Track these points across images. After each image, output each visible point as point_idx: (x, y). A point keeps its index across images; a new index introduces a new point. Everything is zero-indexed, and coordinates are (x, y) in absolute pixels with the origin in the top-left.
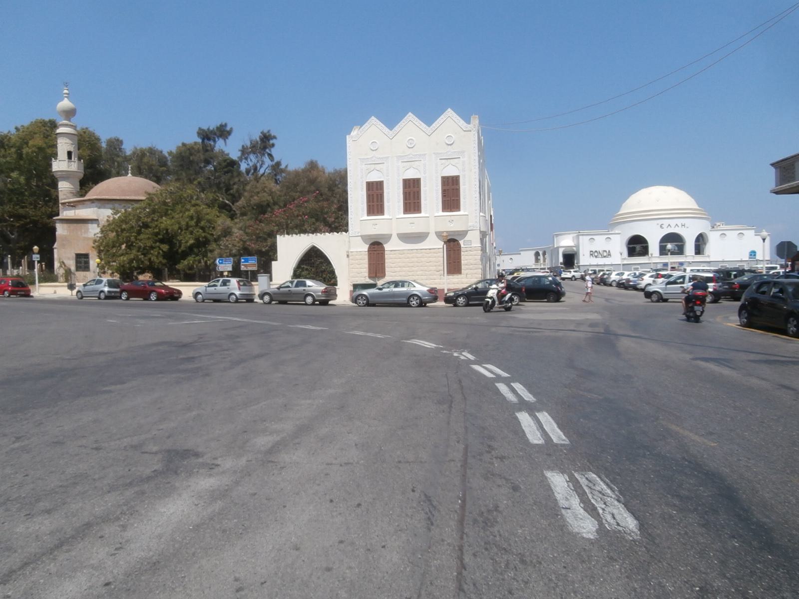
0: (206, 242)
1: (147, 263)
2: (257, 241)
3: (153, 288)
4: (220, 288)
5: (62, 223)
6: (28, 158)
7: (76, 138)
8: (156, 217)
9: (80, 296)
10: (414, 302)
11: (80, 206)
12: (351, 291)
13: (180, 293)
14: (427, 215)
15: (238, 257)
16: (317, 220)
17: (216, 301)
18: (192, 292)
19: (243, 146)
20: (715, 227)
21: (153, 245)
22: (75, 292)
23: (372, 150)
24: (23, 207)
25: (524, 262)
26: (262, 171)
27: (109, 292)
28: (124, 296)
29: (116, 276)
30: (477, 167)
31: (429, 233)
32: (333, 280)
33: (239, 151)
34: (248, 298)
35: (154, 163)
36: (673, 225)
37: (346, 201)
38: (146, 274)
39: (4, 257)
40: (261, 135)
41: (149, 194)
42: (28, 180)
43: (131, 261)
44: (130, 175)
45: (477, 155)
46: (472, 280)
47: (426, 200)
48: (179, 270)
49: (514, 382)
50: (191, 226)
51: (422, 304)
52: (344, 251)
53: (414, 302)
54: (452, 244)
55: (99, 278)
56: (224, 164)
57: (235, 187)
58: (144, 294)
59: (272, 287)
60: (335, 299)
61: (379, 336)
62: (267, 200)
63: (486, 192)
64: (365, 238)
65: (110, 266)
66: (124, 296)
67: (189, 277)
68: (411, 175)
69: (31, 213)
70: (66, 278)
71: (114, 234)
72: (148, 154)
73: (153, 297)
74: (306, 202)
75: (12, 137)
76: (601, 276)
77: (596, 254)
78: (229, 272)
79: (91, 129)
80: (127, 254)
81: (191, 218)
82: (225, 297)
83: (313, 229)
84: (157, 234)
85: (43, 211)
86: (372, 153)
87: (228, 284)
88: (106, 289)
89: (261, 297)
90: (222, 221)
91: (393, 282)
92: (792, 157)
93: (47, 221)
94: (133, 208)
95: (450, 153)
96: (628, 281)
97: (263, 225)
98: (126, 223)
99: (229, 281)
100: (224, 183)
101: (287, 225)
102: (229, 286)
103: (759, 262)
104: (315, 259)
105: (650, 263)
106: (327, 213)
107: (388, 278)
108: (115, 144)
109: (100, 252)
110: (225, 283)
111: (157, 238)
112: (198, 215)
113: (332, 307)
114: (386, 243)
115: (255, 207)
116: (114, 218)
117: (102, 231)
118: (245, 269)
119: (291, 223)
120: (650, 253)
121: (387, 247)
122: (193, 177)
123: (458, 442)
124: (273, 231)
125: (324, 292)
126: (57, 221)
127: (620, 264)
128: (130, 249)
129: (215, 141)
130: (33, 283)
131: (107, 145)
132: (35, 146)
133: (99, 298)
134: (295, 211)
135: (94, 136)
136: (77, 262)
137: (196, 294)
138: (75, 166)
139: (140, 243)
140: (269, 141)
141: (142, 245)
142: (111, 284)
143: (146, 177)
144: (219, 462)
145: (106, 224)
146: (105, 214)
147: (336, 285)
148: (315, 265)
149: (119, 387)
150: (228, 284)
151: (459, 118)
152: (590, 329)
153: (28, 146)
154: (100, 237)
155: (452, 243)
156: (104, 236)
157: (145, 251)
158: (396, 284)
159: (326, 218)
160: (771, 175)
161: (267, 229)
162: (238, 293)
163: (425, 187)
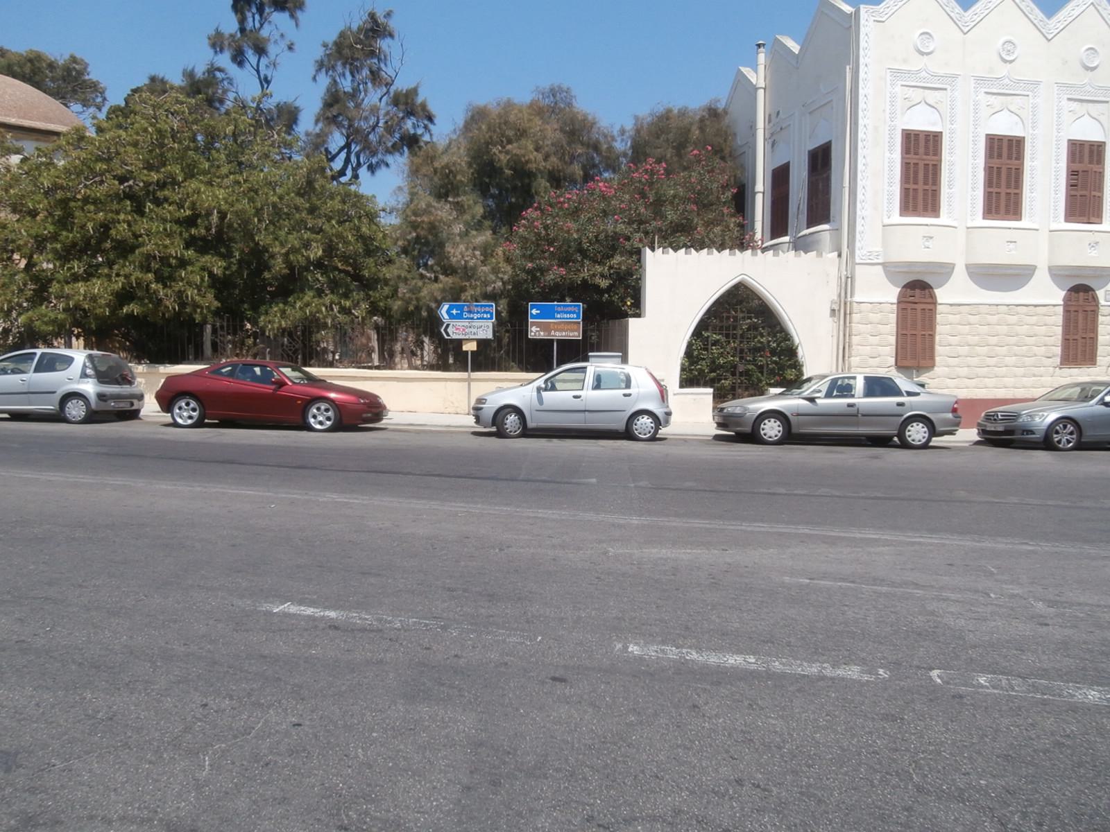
47: (950, 186)
64: (891, 270)
114: (940, 286)
121: (942, 295)
163: (1032, 159)
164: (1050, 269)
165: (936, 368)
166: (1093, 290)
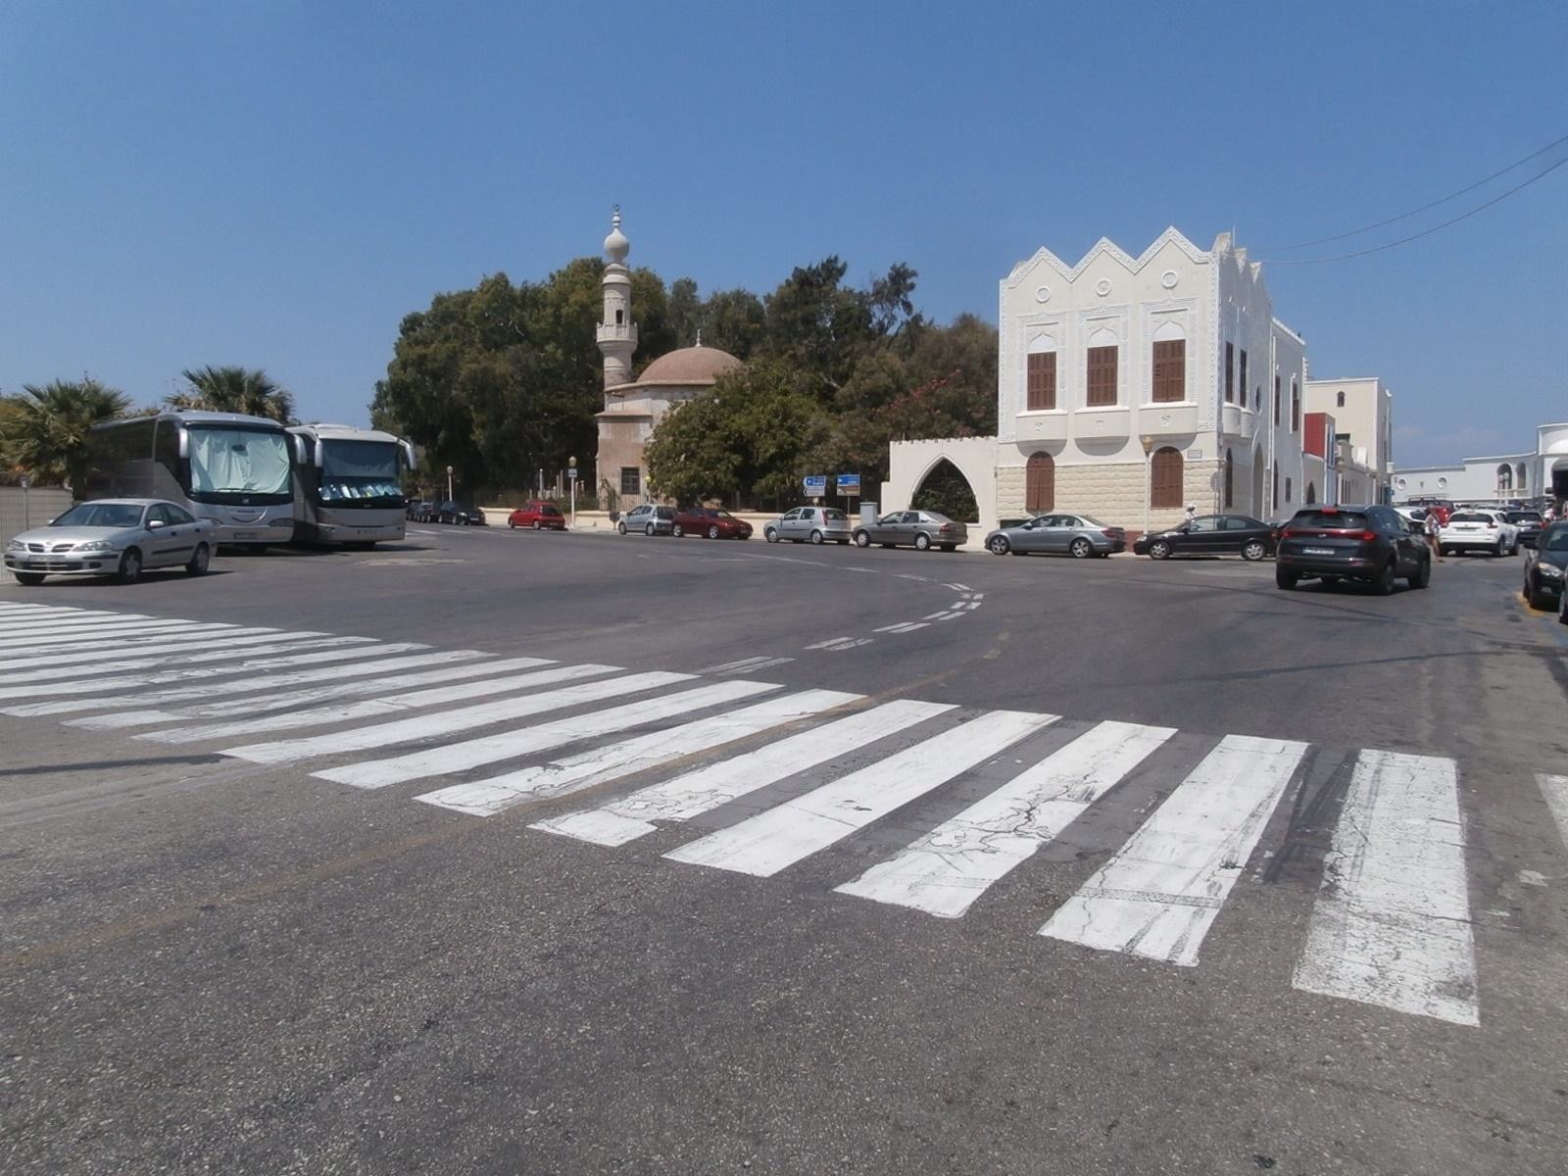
0: (796, 449)
3: (713, 520)
4: (801, 523)
7: (628, 291)
10: (1080, 550)
11: (630, 396)
13: (749, 528)
14: (1126, 408)
17: (797, 541)
26: (891, 331)
28: (677, 531)
39: (535, 473)
43: (692, 479)
44: (698, 345)
47: (1125, 382)
51: (1095, 553)
52: (990, 467)
53: (1080, 550)
54: (1167, 461)
55: (648, 505)
64: (1023, 446)
66: (677, 531)
67: (769, 507)
68: (1101, 341)
69: (569, 405)
73: (713, 533)
75: (547, 289)
79: (650, 270)
82: (805, 535)
84: (727, 439)
86: (1042, 307)
88: (655, 520)
90: (818, 419)
95: (1169, 302)
99: (813, 512)
109: (652, 465)
117: (656, 435)
121: (1059, 461)
124: (886, 435)
125: (945, 530)
130: (569, 511)
131: (674, 293)
133: (646, 532)
136: (624, 481)
140: (904, 280)
142: (661, 513)
146: (659, 408)
153: (567, 304)
154: (654, 444)
157: (710, 465)
162: (823, 529)
163: (1193, 355)
164: (1076, 440)
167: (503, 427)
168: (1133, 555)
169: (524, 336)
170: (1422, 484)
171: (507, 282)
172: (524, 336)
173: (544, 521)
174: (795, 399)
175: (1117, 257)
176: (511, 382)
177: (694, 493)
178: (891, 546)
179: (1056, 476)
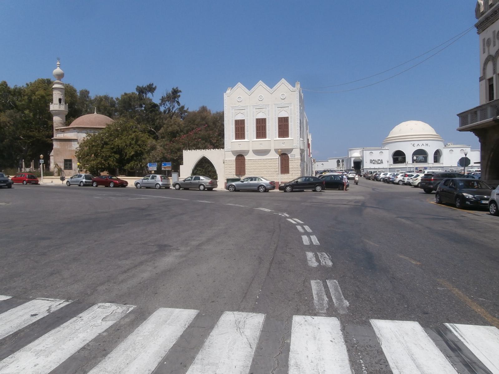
0: (142, 153)
1: (107, 165)
2: (171, 153)
3: (111, 180)
4: (150, 180)
5: (57, 141)
6: (34, 102)
8: (112, 138)
9: (68, 184)
10: (262, 190)
11: (67, 131)
12: (225, 183)
13: (127, 183)
14: (270, 140)
15: (160, 163)
16: (206, 141)
17: (147, 188)
18: (134, 182)
19: (163, 97)
20: (447, 146)
21: (111, 155)
22: (65, 182)
23: (238, 101)
24: (31, 131)
25: (328, 166)
27: (85, 182)
28: (95, 184)
29: (88, 173)
30: (299, 112)
31: (271, 150)
32: (215, 176)
33: (160, 99)
34: (166, 186)
35: (108, 105)
36: (421, 144)
37: (223, 130)
38: (105, 172)
40: (172, 90)
41: (108, 125)
42: (35, 115)
44: (95, 113)
45: (299, 105)
46: (295, 177)
48: (125, 170)
49: (305, 225)
50: (132, 144)
51: (266, 190)
52: (222, 160)
53: (262, 190)
54: (284, 156)
55: (77, 173)
56: (150, 106)
57: (158, 121)
58: (106, 183)
59: (179, 180)
60: (217, 187)
61: (241, 206)
62: (177, 130)
63: (305, 125)
64: (234, 152)
65: (85, 167)
66: (95, 184)
67: (131, 174)
69: (36, 135)
70: (58, 174)
71: (88, 148)
72: (104, 99)
73: (112, 185)
74: (200, 131)
76: (375, 175)
77: (374, 162)
78: (155, 171)
79: (71, 85)
80: (95, 160)
81: (133, 139)
83: (204, 147)
84: (113, 148)
85: (44, 134)
86: (240, 103)
87: (155, 178)
89: (174, 185)
90: (151, 142)
91: (250, 178)
92: (467, 111)
93: (46, 140)
94: (99, 133)
96: (389, 178)
97: (175, 144)
98: (95, 142)
99: (156, 176)
100: (151, 118)
101: (189, 144)
102: (156, 179)
103: (473, 167)
104: (205, 164)
105: (407, 168)
106: (212, 137)
107: (247, 176)
108: (85, 93)
109: (79, 158)
110: (153, 178)
111: (112, 151)
112: (137, 138)
113: (215, 192)
114: (245, 156)
115: (170, 134)
116: (87, 139)
117: (80, 146)
118: (164, 169)
119: (191, 143)
120: (406, 161)
121: (247, 158)
122: (133, 115)
123: (274, 244)
124: (180, 148)
126: (54, 140)
127: (387, 168)
128: (97, 157)
129: (146, 94)
130: (40, 176)
131: (80, 94)
132: (40, 95)
133: (80, 185)
134: (193, 136)
135: (73, 89)
137: (137, 184)
138: (63, 108)
139: (103, 154)
140: (177, 93)
141: (104, 154)
142: (86, 177)
143: (103, 114)
144: (179, 248)
145: (83, 142)
146: (82, 136)
147: (217, 179)
148: (205, 168)
149: (122, 225)
150: (155, 178)
151: (289, 84)
152: (354, 204)
154: (79, 150)
155: (284, 156)
156: (82, 149)
157: (106, 158)
158: (252, 179)
159: (211, 140)
160: (457, 121)
161: (177, 146)
162: (160, 183)
165: (246, 175)
166: (287, 154)
167: (4, 143)
168: (278, 190)
169: (14, 106)
170: (318, 165)
171: (7, 85)
172: (14, 106)
173: (28, 181)
174: (140, 134)
175: (265, 88)
176: (9, 125)
177: (98, 169)
178: (187, 189)
179: (246, 163)
